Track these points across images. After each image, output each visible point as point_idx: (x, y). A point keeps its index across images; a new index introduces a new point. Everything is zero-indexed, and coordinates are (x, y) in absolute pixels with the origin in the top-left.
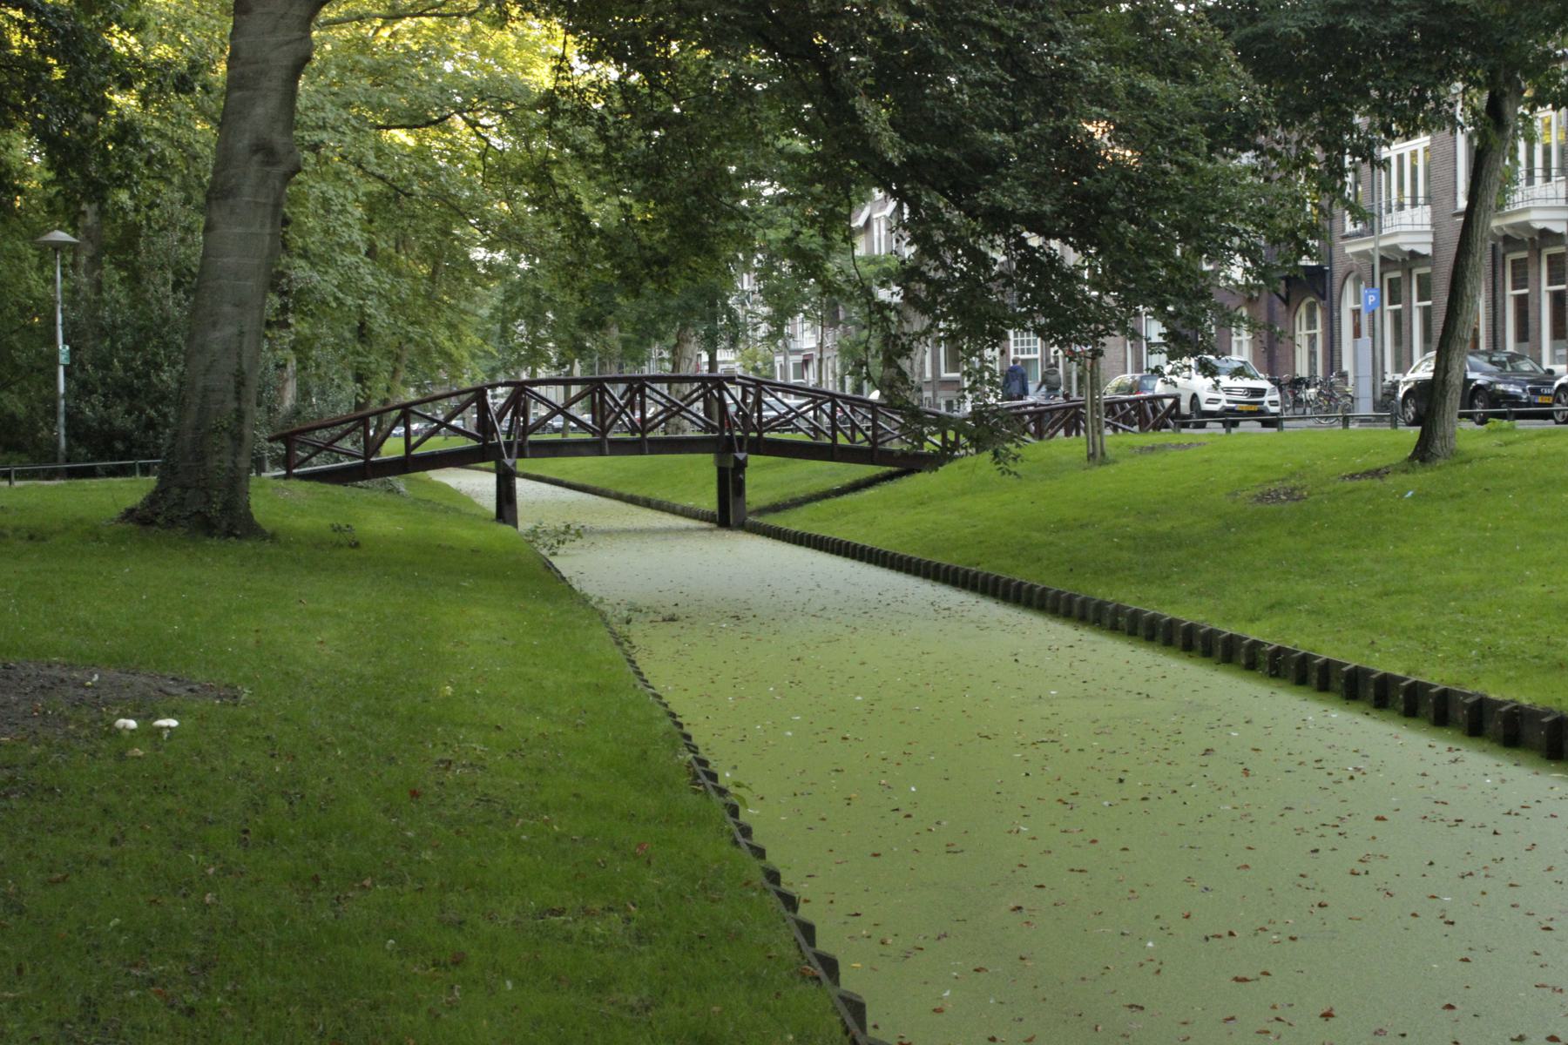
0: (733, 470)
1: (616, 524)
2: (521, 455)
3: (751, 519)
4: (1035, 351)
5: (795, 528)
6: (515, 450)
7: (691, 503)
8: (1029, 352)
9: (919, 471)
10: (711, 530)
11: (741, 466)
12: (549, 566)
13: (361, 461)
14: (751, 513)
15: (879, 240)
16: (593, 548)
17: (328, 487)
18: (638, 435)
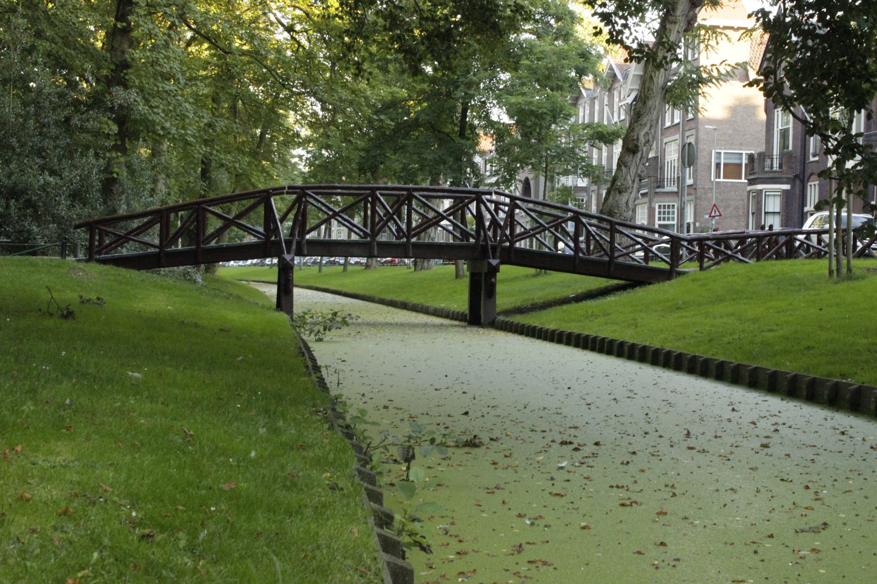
0: (486, 274)
1: (381, 319)
2: (300, 253)
3: (501, 318)
4: (673, 219)
5: (552, 326)
6: (294, 247)
7: (442, 305)
8: (668, 219)
9: (650, 284)
10: (465, 327)
11: (494, 271)
12: (305, 351)
13: (157, 250)
14: (499, 314)
15: (584, 116)
16: (358, 336)
17: (123, 271)
18: (405, 240)
